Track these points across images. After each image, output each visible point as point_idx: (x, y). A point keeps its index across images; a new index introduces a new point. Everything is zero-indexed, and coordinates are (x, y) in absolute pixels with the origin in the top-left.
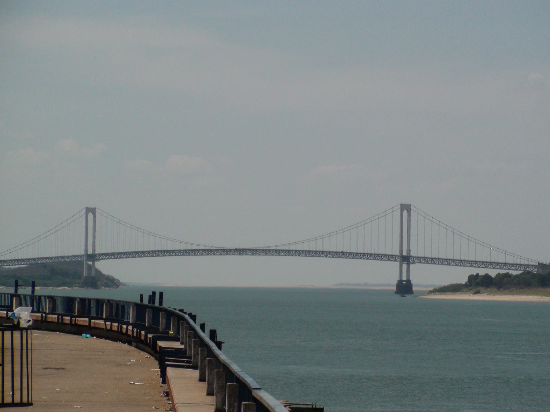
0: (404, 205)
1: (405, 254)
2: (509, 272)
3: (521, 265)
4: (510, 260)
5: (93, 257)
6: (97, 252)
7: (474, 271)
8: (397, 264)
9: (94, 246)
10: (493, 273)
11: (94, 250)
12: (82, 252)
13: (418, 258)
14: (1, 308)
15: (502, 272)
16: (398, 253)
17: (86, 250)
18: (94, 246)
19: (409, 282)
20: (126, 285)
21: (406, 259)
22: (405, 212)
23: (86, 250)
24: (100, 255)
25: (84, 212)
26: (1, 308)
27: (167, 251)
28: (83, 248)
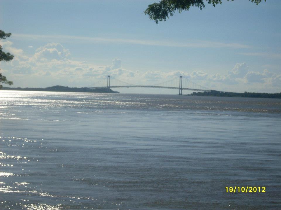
0: (69, 88)
1: (109, 86)
2: (3, 85)
3: (204, 90)
4: (201, 89)
5: (109, 87)
6: (111, 86)
7: (194, 91)
8: (179, 90)
9: (110, 84)
10: (197, 92)
11: (110, 85)
12: (107, 86)
13: (184, 88)
14: (280, 204)
15: (199, 92)
16: (179, 87)
17: (108, 85)
18: (110, 84)
19: (181, 94)
20: (119, 93)
21: (181, 89)
22: (109, 78)
23: (108, 85)
24: (111, 87)
25: (107, 77)
26: (280, 204)
27: (121, 86)
28: (107, 85)
